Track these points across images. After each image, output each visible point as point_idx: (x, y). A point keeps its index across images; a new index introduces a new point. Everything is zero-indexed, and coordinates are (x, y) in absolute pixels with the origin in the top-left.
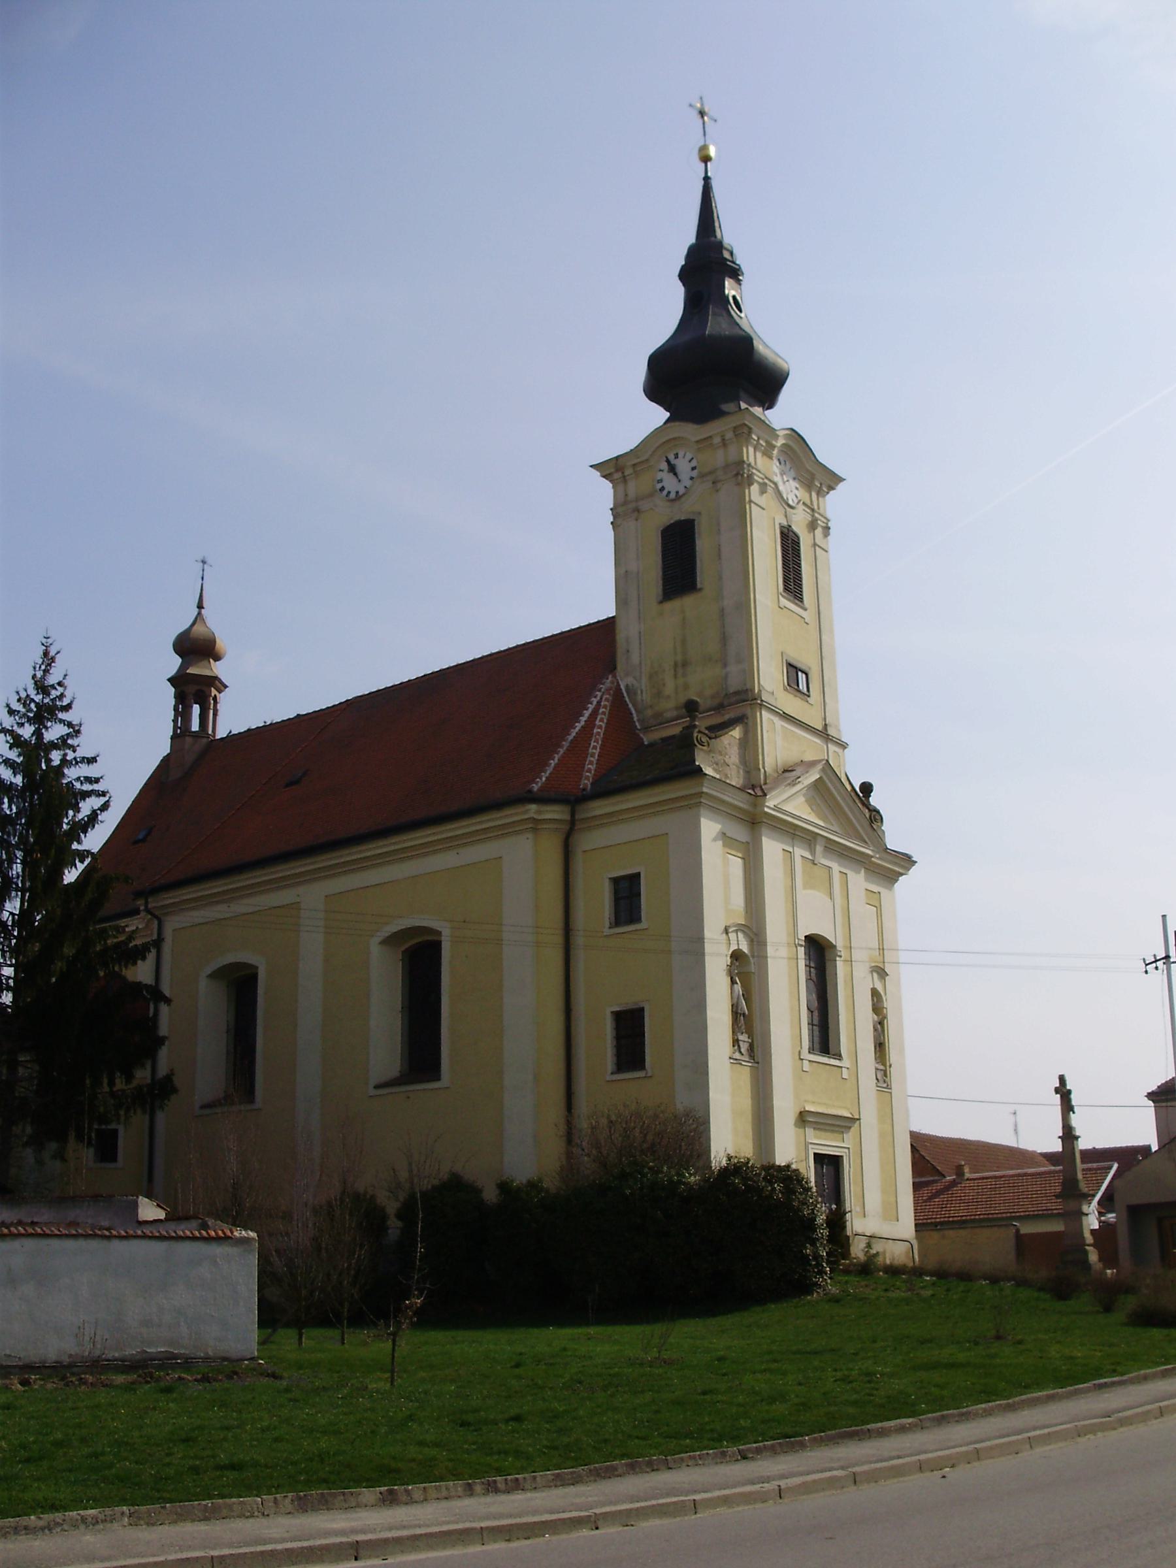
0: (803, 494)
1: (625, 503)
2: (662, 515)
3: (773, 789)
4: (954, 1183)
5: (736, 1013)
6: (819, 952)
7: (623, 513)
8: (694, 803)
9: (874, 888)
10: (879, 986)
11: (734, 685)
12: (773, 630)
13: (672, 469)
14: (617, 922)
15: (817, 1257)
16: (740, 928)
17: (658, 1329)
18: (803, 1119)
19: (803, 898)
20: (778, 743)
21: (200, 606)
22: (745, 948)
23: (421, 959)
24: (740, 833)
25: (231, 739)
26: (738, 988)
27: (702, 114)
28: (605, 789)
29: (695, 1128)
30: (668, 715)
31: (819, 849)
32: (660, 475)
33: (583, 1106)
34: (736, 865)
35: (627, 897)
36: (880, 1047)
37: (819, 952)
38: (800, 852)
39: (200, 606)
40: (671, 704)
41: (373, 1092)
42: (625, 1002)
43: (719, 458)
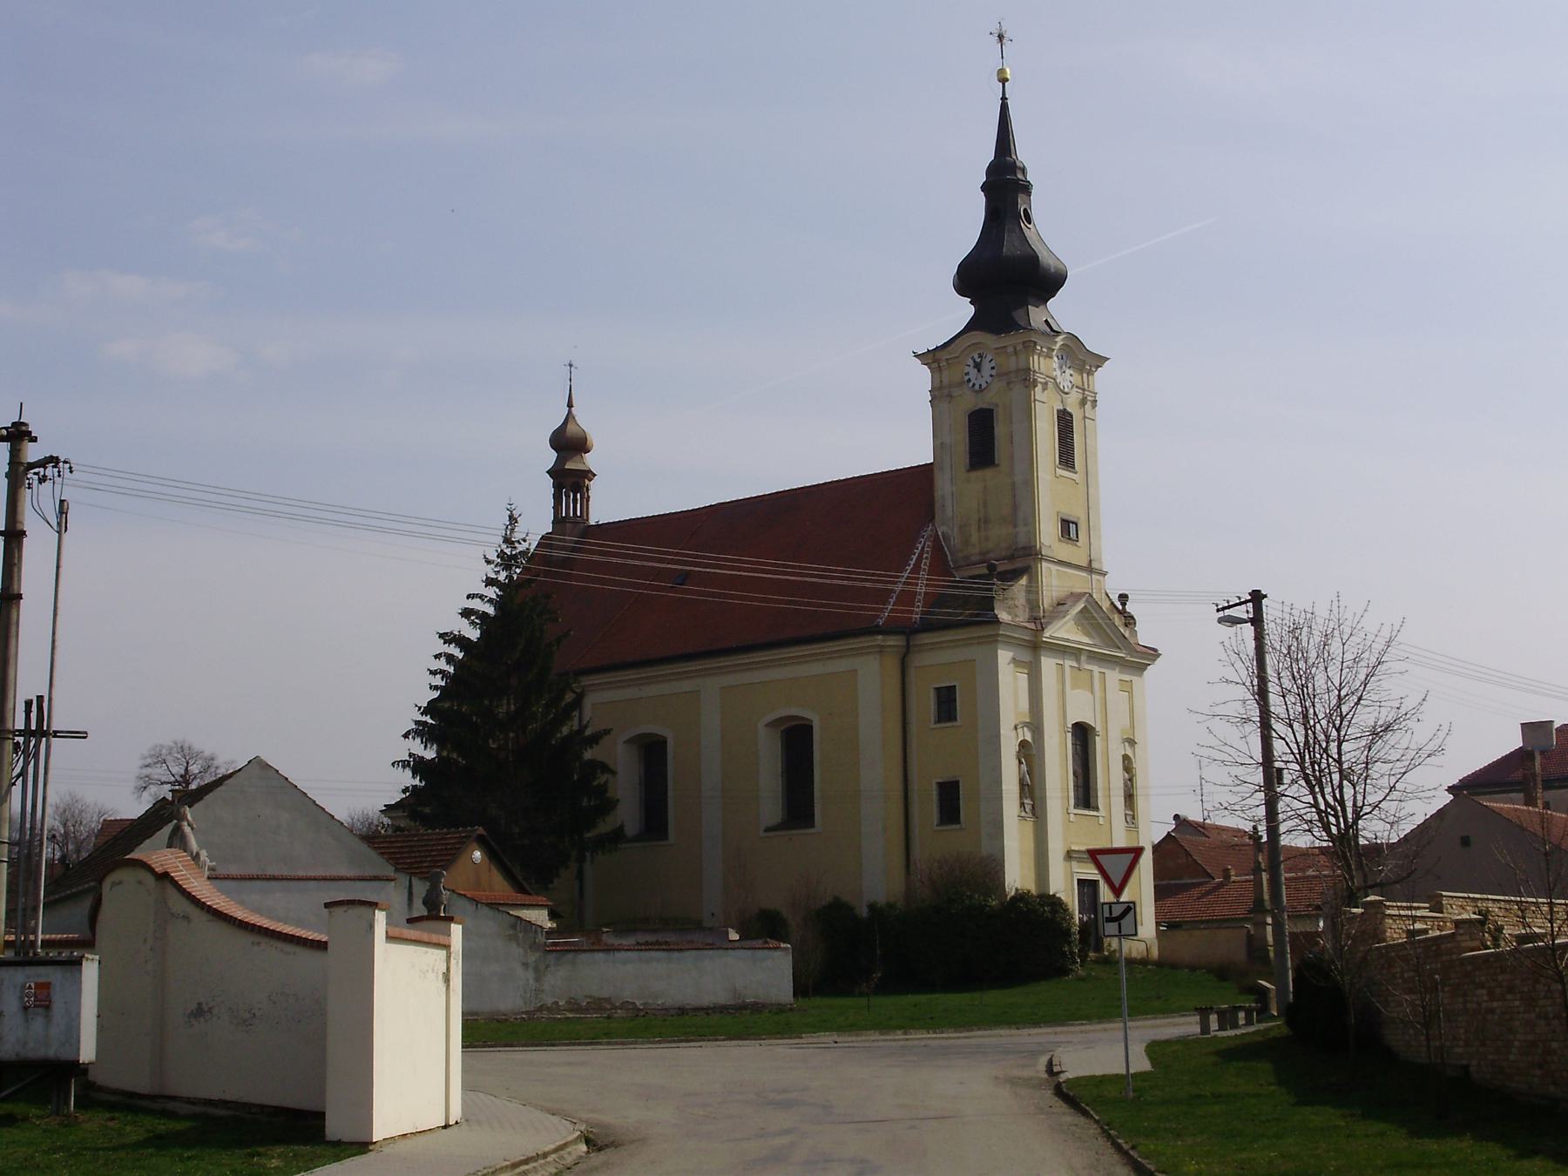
0: (1076, 379)
1: (940, 388)
2: (969, 402)
3: (1049, 623)
4: (1220, 885)
5: (1022, 784)
6: (1083, 735)
7: (939, 395)
8: (994, 641)
9: (1127, 677)
10: (1129, 753)
11: (1022, 541)
12: (1051, 493)
13: (978, 366)
14: (939, 720)
15: (1072, 953)
16: (1026, 725)
17: (976, 995)
18: (1070, 855)
19: (1069, 696)
20: (1053, 582)
21: (570, 405)
22: (1029, 739)
23: (797, 740)
24: (1026, 656)
25: (598, 526)
26: (1024, 767)
27: (1001, 37)
28: (928, 626)
29: (993, 868)
30: (974, 558)
31: (1083, 658)
32: (967, 369)
33: (916, 852)
34: (1023, 679)
35: (946, 703)
36: (1130, 798)
37: (1083, 735)
38: (1069, 663)
39: (570, 405)
40: (976, 550)
41: (762, 834)
42: (945, 776)
43: (1012, 363)
